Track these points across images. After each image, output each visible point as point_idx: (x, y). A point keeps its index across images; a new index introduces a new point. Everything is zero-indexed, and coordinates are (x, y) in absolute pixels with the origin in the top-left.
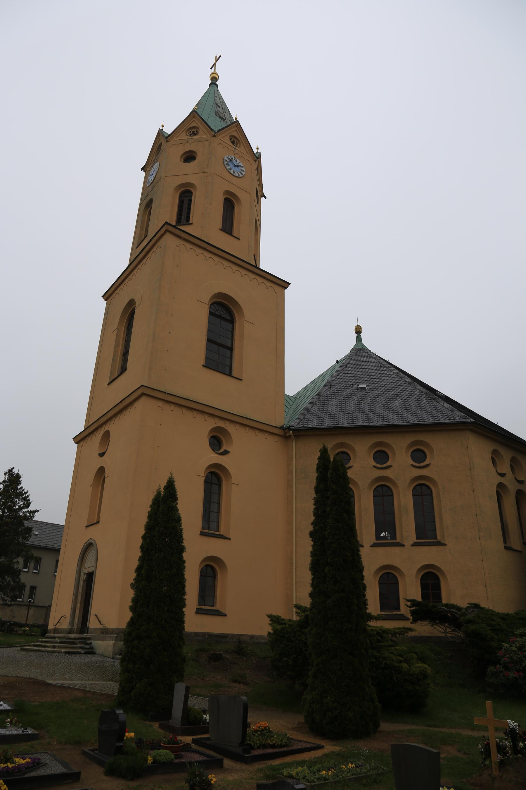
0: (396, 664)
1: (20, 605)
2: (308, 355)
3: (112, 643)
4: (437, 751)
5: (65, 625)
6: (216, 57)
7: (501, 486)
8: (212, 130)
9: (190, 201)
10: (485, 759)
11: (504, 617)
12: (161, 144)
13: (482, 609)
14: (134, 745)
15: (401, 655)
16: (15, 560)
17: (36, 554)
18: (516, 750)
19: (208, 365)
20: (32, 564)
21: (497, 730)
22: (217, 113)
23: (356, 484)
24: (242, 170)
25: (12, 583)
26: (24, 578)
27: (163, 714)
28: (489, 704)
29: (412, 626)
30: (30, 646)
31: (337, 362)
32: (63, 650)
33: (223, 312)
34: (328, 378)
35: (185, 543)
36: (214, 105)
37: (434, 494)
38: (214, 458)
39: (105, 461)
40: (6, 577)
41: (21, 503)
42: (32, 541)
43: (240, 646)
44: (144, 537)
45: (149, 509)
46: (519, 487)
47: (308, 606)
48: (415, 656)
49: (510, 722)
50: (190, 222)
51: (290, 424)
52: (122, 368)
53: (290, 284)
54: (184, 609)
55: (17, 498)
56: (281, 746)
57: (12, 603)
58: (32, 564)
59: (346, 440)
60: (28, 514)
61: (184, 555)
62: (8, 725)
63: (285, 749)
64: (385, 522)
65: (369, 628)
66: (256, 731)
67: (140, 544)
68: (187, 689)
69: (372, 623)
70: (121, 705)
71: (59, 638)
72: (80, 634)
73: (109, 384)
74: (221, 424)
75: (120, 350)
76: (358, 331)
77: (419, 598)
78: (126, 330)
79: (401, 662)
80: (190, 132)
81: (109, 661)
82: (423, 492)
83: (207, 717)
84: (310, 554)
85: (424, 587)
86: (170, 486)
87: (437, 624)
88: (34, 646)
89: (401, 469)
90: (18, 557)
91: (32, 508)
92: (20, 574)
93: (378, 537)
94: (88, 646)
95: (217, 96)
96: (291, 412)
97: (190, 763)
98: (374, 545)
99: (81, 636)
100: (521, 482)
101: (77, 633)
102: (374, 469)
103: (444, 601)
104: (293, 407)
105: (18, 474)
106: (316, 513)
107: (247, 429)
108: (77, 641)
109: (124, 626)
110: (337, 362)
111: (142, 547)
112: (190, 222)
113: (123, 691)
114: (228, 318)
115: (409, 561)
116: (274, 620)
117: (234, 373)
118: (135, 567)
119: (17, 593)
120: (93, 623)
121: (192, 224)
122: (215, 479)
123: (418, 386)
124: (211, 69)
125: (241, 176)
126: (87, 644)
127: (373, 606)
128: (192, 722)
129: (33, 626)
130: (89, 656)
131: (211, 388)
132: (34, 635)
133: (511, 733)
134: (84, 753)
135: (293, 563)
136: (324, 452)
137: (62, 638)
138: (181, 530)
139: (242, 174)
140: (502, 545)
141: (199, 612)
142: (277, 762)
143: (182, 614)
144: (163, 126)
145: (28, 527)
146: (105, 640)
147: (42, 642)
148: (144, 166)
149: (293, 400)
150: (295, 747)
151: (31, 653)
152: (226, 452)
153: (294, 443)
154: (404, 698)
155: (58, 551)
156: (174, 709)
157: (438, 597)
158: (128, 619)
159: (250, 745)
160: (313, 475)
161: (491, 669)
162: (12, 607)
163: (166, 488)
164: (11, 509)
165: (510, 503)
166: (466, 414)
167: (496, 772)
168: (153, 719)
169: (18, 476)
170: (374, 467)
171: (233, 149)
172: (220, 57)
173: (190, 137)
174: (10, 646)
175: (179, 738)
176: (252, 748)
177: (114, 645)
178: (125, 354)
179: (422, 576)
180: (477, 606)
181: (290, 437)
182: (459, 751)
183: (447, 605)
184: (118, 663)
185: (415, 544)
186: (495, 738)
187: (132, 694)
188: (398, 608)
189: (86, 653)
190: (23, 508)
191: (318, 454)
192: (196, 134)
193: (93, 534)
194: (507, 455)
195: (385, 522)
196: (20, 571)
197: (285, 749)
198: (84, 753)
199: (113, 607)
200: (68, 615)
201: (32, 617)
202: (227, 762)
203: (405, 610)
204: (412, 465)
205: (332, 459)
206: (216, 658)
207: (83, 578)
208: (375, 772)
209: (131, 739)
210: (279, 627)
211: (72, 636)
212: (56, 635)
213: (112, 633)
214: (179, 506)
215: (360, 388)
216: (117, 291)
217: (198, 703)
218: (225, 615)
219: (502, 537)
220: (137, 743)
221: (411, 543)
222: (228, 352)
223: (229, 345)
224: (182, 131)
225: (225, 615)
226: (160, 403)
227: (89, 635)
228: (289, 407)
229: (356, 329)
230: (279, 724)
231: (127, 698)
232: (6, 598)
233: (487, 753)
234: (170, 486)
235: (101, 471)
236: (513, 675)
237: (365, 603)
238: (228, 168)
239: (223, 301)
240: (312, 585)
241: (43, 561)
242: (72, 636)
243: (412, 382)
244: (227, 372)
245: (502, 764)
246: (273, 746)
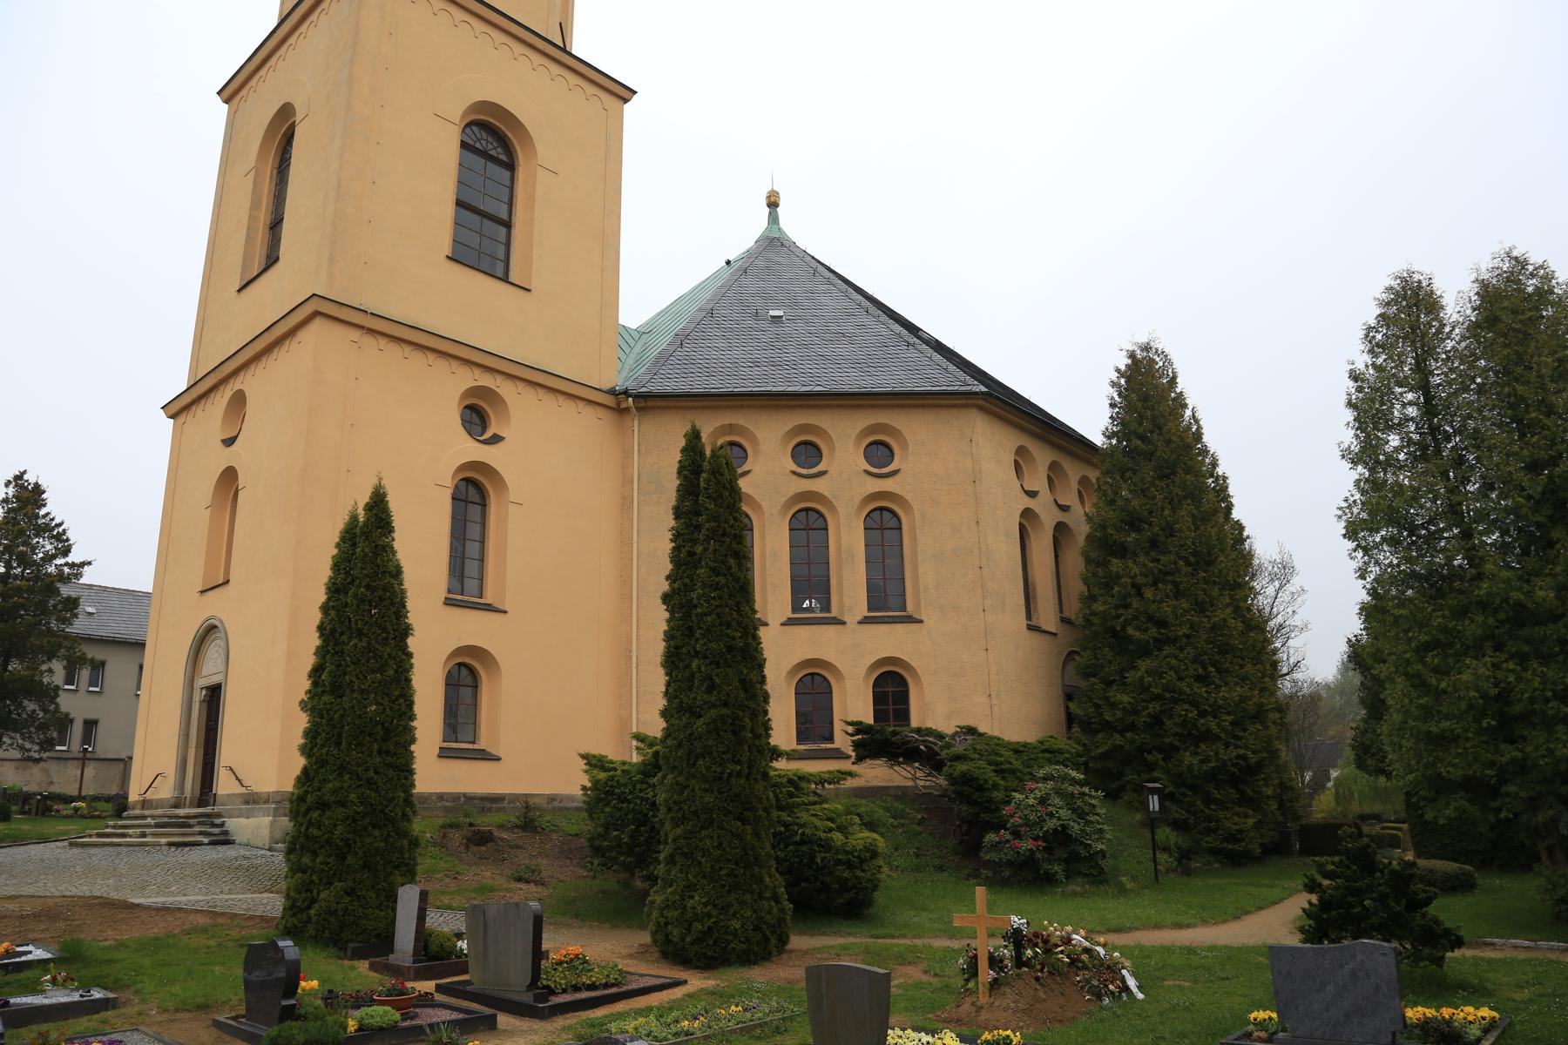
0: (823, 835)
1: (61, 759)
2: (665, 254)
3: (267, 820)
4: (882, 971)
5: (165, 791)
7: (1027, 514)
10: (967, 980)
11: (1018, 749)
13: (981, 735)
14: (319, 1002)
15: (831, 820)
16: (44, 667)
17: (92, 652)
18: (1019, 962)
20: (85, 673)
21: (992, 936)
23: (756, 506)
25: (41, 715)
26: (65, 703)
27: (378, 944)
28: (980, 891)
29: (855, 768)
31: (728, 263)
32: (164, 840)
33: (492, 141)
34: (708, 296)
35: (412, 619)
37: (905, 527)
39: (236, 456)
40: (26, 702)
41: (49, 547)
42: (79, 626)
43: (529, 817)
44: (325, 608)
45: (335, 551)
46: (1061, 517)
47: (659, 735)
48: (857, 820)
49: (1014, 918)
51: (630, 384)
52: (268, 257)
53: (635, 92)
54: (413, 748)
55: (37, 536)
56: (606, 986)
57: (45, 755)
58: (85, 673)
59: (740, 419)
60: (66, 570)
61: (410, 641)
62: (48, 986)
63: (613, 992)
64: (812, 584)
65: (772, 773)
66: (560, 963)
67: (317, 622)
68: (424, 896)
69: (781, 764)
70: (289, 932)
71: (152, 817)
72: (199, 806)
74: (486, 381)
75: (264, 217)
76: (773, 204)
77: (869, 720)
79: (831, 830)
81: (263, 856)
82: (884, 521)
83: (463, 945)
84: (662, 636)
85: (879, 699)
86: (378, 504)
87: (899, 764)
88: (99, 835)
89: (845, 479)
90: (50, 660)
91: (73, 557)
92: (57, 695)
93: (796, 607)
94: (216, 830)
96: (630, 361)
97: (431, 1026)
98: (789, 622)
99: (200, 810)
101: (191, 805)
103: (915, 723)
104: (637, 349)
105: (37, 486)
106: (675, 557)
107: (541, 392)
108: (192, 821)
109: (288, 786)
110: (728, 263)
111: (321, 628)
113: (292, 908)
114: (503, 157)
115: (853, 652)
116: (595, 763)
118: (309, 668)
119: (55, 735)
120: (224, 785)
122: (473, 493)
123: (884, 318)
126: (213, 825)
127: (783, 732)
128: (434, 955)
129: (96, 798)
130: (220, 848)
132: (99, 817)
133: (1016, 938)
134: (218, 1025)
136: (694, 437)
138: (403, 592)
140: (1025, 623)
141: (445, 754)
142: (599, 1013)
143: (410, 756)
145: (69, 598)
147: (114, 827)
149: (636, 336)
150: (634, 986)
151: (94, 851)
152: (496, 439)
154: (833, 891)
155: (141, 645)
156: (397, 935)
157: (903, 715)
158: (297, 771)
159: (548, 987)
160: (672, 483)
161: (991, 837)
162: (42, 764)
163: (369, 508)
164: (24, 560)
165: (1042, 546)
167: (984, 999)
168: (358, 955)
169: (38, 490)
170: (794, 473)
174: (45, 840)
175: (409, 985)
176: (552, 992)
177: (272, 823)
178: (276, 225)
180: (971, 731)
181: (627, 410)
182: (926, 972)
183: (918, 731)
184: (280, 858)
185: (866, 621)
186: (985, 945)
187: (312, 912)
188: (831, 739)
189: (211, 843)
190: (54, 557)
191: (683, 443)
193: (217, 606)
194: (1042, 456)
195: (812, 584)
196: (57, 688)
197: (613, 992)
198: (218, 1025)
199: (266, 749)
200: (171, 771)
201: (94, 781)
202: (503, 1020)
203: (842, 740)
204: (866, 472)
205: (708, 453)
206: (481, 839)
207: (198, 696)
208: (780, 1015)
209: (312, 993)
210: (602, 776)
211: (181, 812)
212: (146, 812)
213: (267, 802)
214: (396, 545)
216: (253, 82)
217: (442, 922)
218: (499, 759)
220: (325, 999)
221: (859, 618)
222: (502, 230)
223: (504, 216)
225: (499, 759)
226: (355, 334)
227: (217, 809)
228: (627, 350)
230: (608, 949)
231: (301, 919)
232: (28, 745)
233: (972, 970)
234: (378, 504)
236: (1026, 845)
237: (767, 727)
240: (666, 693)
241: (108, 667)
242: (181, 812)
243: (873, 309)
244: (500, 273)
245: (995, 985)
246: (592, 987)
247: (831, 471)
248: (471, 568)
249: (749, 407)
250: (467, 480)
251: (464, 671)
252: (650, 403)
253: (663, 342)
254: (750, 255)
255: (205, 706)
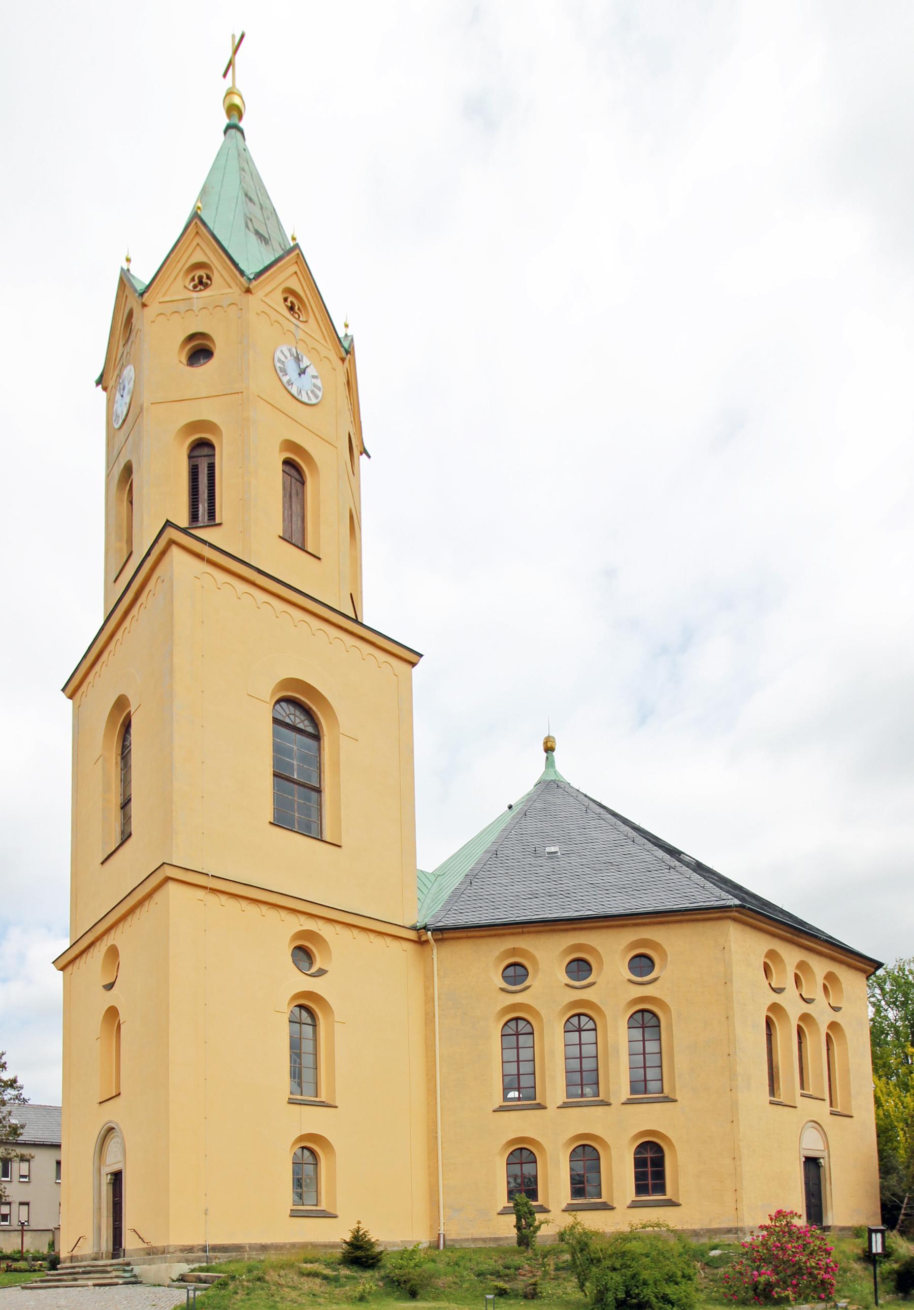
2: (451, 802)
6: (233, 36)
7: (775, 1008)
8: (242, 273)
9: (211, 468)
12: (130, 315)
19: (281, 821)
22: (248, 221)
24: (315, 385)
30: (36, 1282)
31: (510, 807)
32: (90, 1283)
33: (300, 713)
34: (493, 837)
36: (242, 197)
38: (303, 983)
50: (217, 521)
52: (123, 833)
72: (113, 1258)
73: (102, 863)
75: (115, 800)
76: (549, 749)
78: (119, 758)
80: (193, 279)
88: (42, 1281)
89: (613, 986)
93: (505, 1098)
95: (246, 168)
96: (428, 901)
100: (836, 1009)
101: (107, 1258)
102: (568, 989)
108: (109, 1269)
112: (217, 521)
114: (310, 729)
117: (327, 836)
120: (129, 1242)
121: (220, 524)
123: (650, 846)
124: (225, 76)
125: (314, 401)
126: (125, 1271)
131: (290, 863)
135: (436, 1138)
137: (85, 1267)
139: (317, 397)
144: (128, 260)
146: (154, 1264)
148: (102, 376)
149: (433, 879)
152: (321, 972)
153: (435, 951)
155: (58, 1146)
166: (727, 892)
171: (293, 328)
172: (242, 37)
173: (195, 295)
179: (638, 1147)
181: (427, 941)
192: (206, 286)
193: (113, 1113)
207: (106, 1180)
215: (549, 853)
219: (767, 1087)
222: (314, 795)
224: (174, 274)
227: (127, 1259)
229: (546, 743)
235: (112, 1013)
238: (285, 379)
239: (302, 698)
247: (599, 981)
248: (307, 1075)
249: (529, 932)
250: (300, 1006)
251: (306, 1153)
252: (445, 936)
253: (455, 881)
254: (530, 799)
255: (111, 1187)
